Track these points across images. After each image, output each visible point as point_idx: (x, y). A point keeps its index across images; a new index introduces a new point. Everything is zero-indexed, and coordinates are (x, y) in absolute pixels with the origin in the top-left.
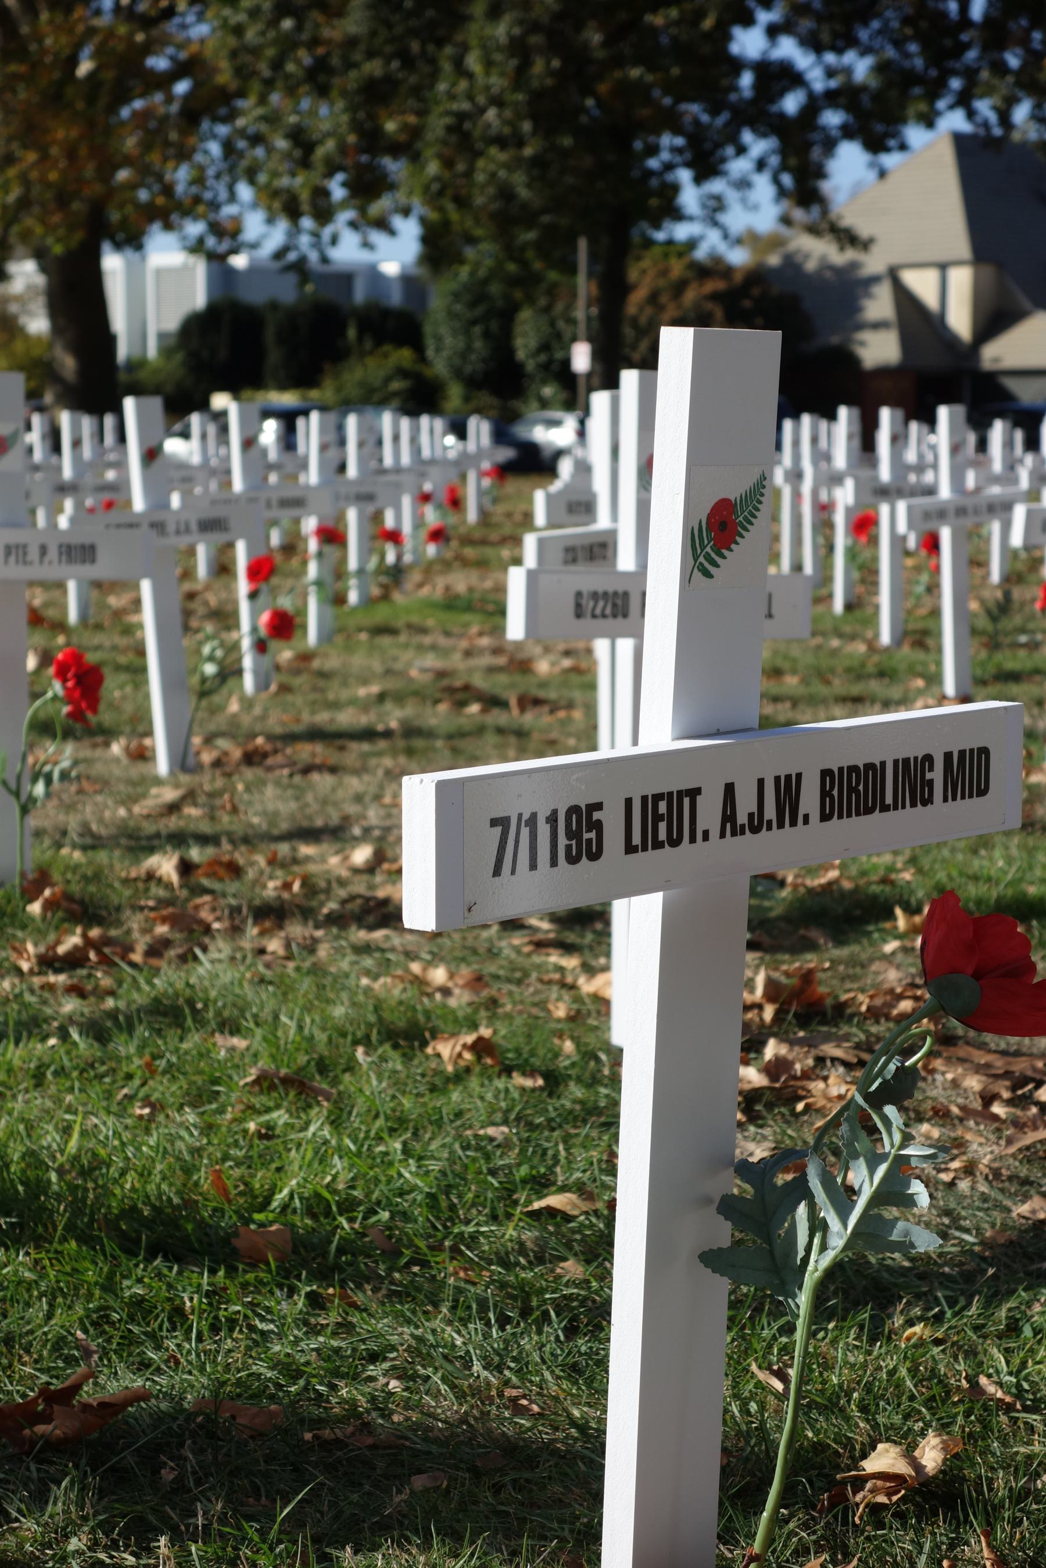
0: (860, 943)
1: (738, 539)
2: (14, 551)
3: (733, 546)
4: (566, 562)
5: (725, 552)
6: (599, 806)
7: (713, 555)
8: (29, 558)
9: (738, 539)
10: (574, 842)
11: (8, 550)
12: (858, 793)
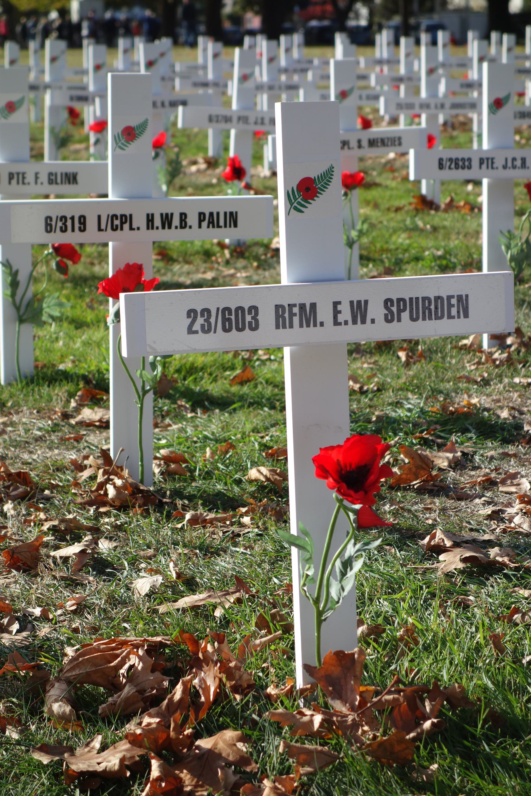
0: (93, 409)
1: (318, 195)
2: (16, 176)
3: (315, 198)
4: (77, 174)
5: (310, 201)
6: (340, 303)
7: (303, 202)
8: (26, 181)
9: (318, 195)
10: (227, 317)
11: (11, 176)
12: (430, 310)
